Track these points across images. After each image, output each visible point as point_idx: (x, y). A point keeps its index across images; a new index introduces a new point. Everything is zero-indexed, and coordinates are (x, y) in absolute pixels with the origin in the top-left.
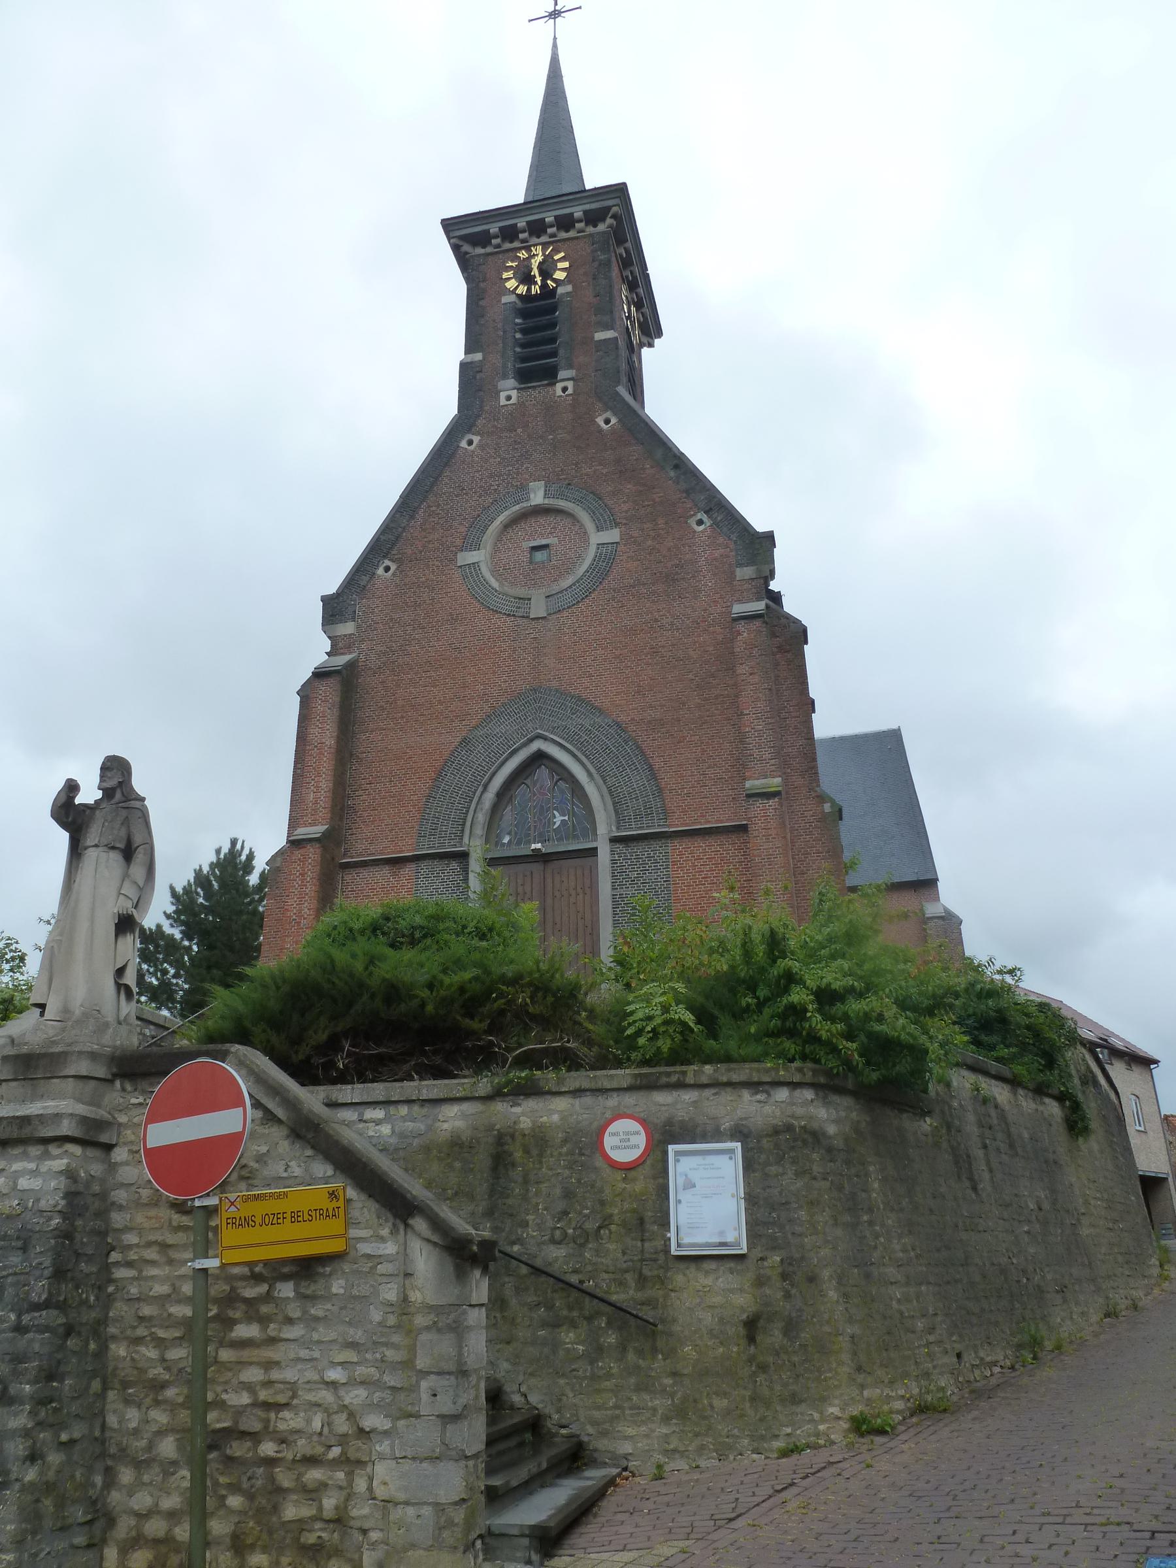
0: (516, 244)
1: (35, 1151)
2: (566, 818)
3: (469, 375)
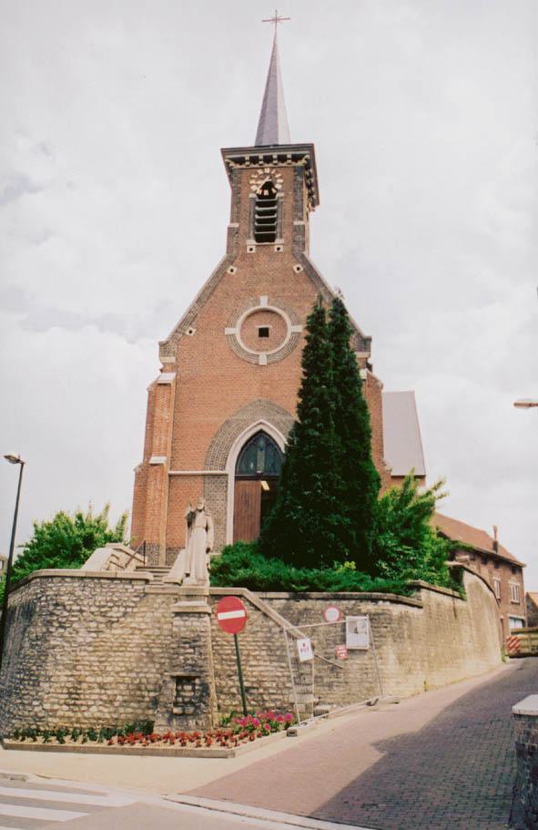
0: (257, 166)
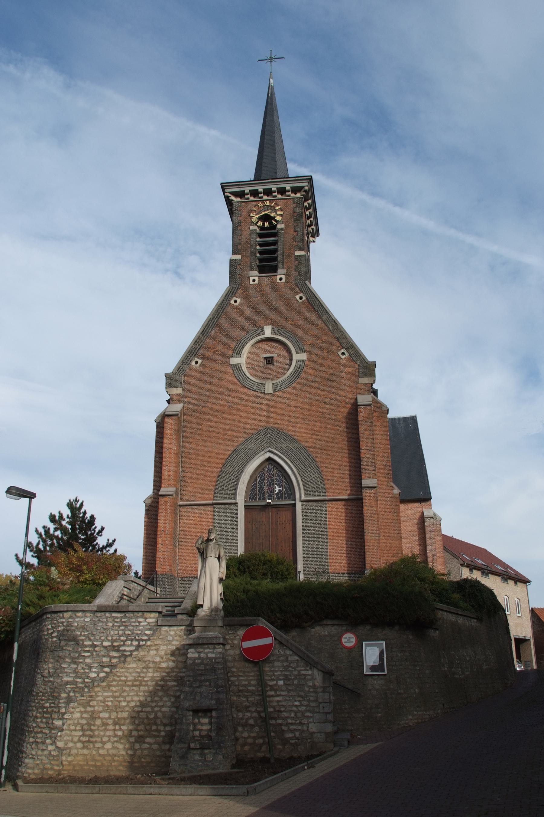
1: (211, 646)
2: (281, 489)
3: (234, 267)
